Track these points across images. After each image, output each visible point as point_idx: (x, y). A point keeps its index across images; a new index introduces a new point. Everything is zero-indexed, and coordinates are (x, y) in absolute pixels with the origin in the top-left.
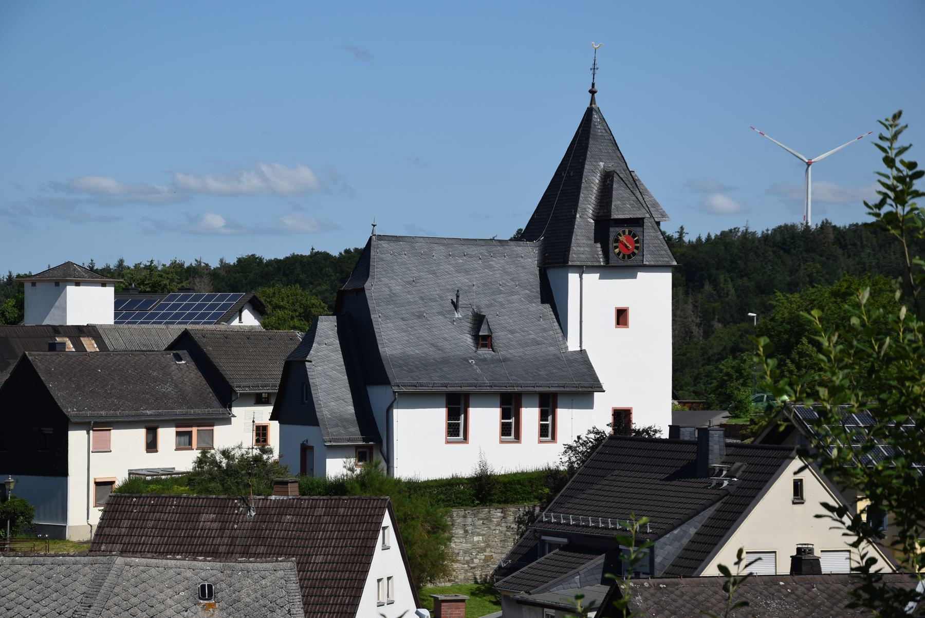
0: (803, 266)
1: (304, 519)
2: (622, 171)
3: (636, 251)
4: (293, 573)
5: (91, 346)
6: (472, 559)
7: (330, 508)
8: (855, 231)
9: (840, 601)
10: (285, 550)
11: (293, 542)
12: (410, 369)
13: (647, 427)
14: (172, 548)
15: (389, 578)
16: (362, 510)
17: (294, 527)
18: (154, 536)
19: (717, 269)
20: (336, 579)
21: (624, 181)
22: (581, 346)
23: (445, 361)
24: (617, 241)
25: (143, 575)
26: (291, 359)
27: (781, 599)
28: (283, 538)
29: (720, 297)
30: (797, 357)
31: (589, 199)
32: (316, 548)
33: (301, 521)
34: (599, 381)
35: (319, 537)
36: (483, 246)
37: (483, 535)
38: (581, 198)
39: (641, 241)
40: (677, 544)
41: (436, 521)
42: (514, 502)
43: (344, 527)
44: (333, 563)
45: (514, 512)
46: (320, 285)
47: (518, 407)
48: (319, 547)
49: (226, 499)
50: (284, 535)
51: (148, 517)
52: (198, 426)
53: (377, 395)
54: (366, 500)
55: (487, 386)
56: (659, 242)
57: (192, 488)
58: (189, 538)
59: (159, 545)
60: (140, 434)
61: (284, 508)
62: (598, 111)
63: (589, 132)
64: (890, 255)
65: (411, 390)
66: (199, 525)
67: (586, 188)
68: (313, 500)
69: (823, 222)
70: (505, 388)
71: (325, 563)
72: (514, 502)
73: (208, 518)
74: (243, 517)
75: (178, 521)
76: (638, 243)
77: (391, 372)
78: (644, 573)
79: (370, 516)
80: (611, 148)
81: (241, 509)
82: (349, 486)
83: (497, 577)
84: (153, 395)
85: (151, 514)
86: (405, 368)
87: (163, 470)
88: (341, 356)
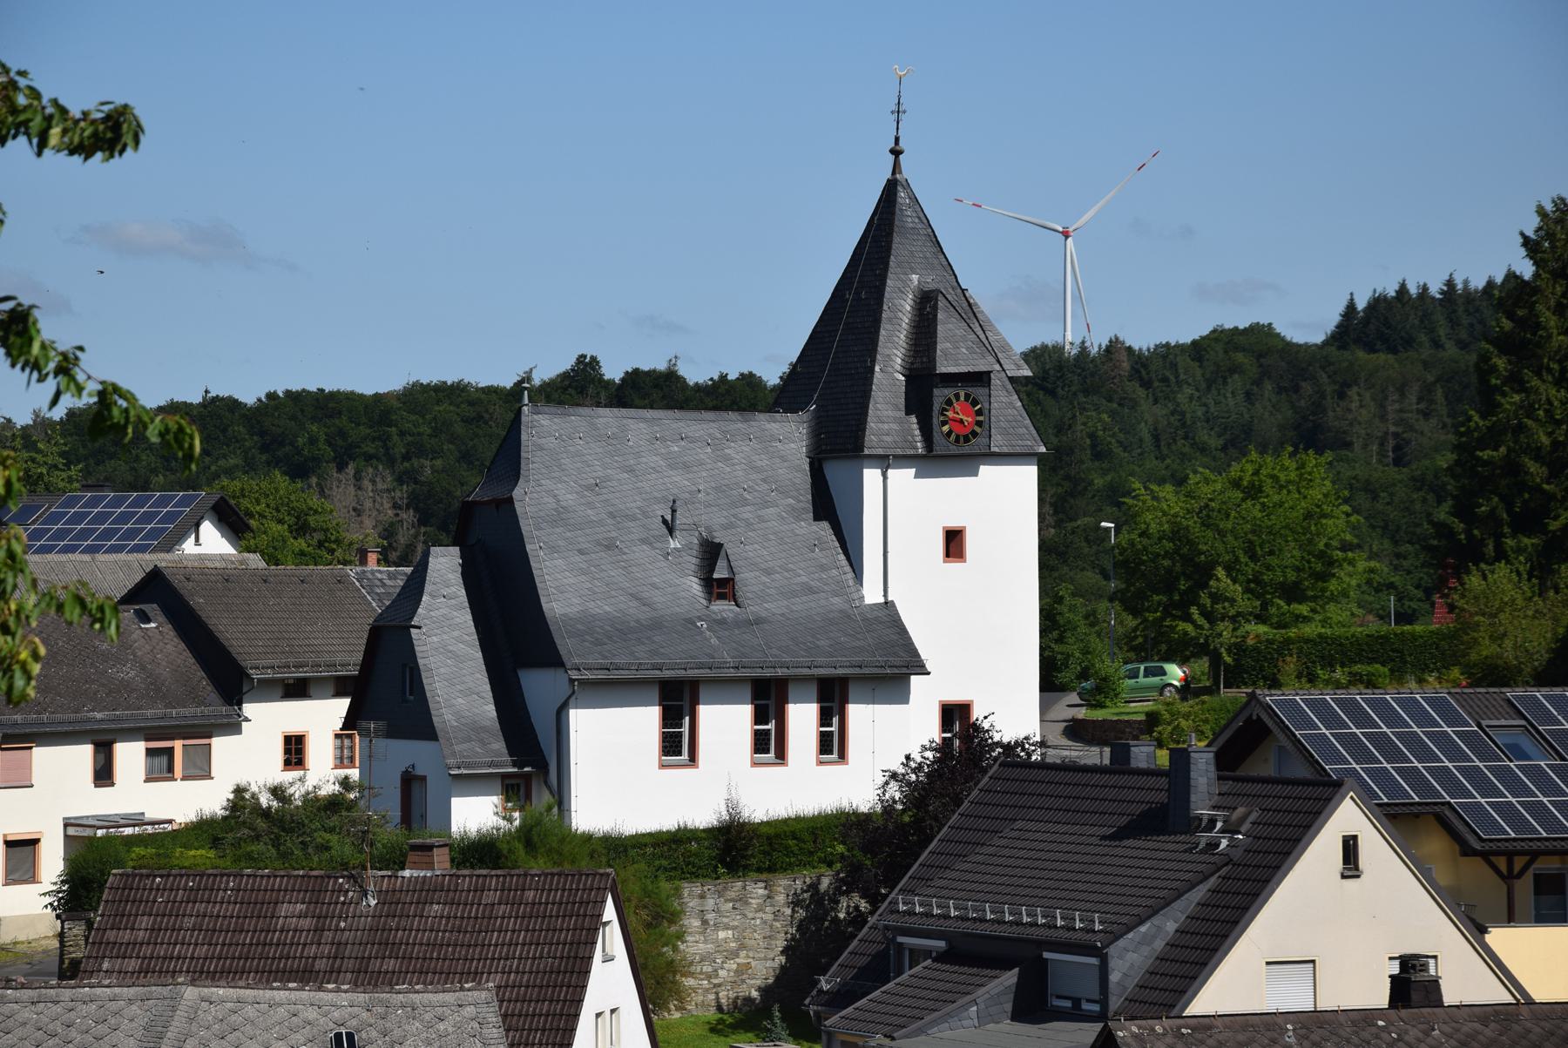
0: (1080, 419)
1: (463, 911)
2: (950, 290)
3: (978, 429)
4: (492, 1009)
6: (716, 971)
7: (510, 890)
8: (1165, 357)
10: (433, 965)
11: (447, 951)
13: (1022, 736)
14: (231, 965)
15: (613, 1011)
16: (566, 894)
17: (447, 925)
18: (196, 944)
20: (527, 1015)
21: (954, 308)
22: (885, 595)
23: (656, 625)
25: (233, 1017)
26: (381, 623)
28: (555, 958)
30: (1208, 602)
31: (896, 339)
32: (488, 961)
33: (459, 915)
34: (919, 656)
35: (493, 942)
37: (734, 928)
38: (881, 338)
39: (987, 412)
40: (1146, 950)
41: (660, 906)
42: (785, 868)
43: (535, 923)
44: (520, 987)
45: (785, 886)
46: (225, 456)
47: (782, 702)
48: (493, 959)
50: (429, 939)
51: (185, 910)
52: (184, 738)
53: (538, 686)
54: (573, 875)
56: (1016, 413)
58: (260, 947)
59: (206, 959)
60: (83, 754)
61: (428, 890)
62: (907, 186)
63: (891, 224)
64: (1226, 397)
65: (601, 675)
66: (277, 924)
67: (890, 320)
68: (478, 876)
69: (1111, 341)
71: (506, 987)
72: (785, 870)
73: (291, 911)
74: (355, 909)
75: (238, 917)
77: (566, 645)
78: (1088, 1001)
79: (581, 903)
80: (929, 250)
81: (351, 894)
82: (504, 847)
83: (815, 1008)
84: (103, 685)
85: (190, 905)
87: (125, 817)
88: (470, 617)
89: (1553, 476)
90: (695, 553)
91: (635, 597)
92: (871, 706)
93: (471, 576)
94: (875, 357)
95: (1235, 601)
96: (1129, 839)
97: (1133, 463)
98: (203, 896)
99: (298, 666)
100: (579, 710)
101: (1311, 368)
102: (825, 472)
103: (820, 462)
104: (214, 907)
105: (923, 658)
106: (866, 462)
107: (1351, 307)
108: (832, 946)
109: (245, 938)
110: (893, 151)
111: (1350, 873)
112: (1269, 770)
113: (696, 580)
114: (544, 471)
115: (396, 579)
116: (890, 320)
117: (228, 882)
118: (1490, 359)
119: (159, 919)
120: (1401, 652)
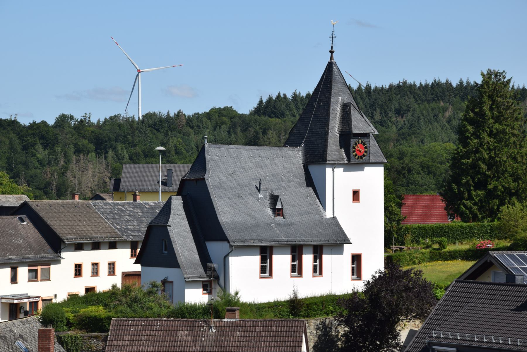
0: (171, 140)
3: (365, 154)
7: (266, 326)
8: (198, 118)
12: (238, 231)
18: (148, 346)
19: (116, 142)
22: (333, 215)
23: (257, 226)
24: (354, 148)
26: (152, 224)
29: (119, 159)
34: (347, 237)
38: (330, 120)
42: (314, 316)
49: (193, 321)
52: (41, 266)
55: (284, 241)
57: (109, 311)
58: (173, 347)
61: (235, 326)
62: (336, 64)
65: (241, 244)
66: (178, 339)
69: (178, 112)
70: (295, 242)
77: (229, 233)
81: (205, 328)
84: (12, 246)
85: (144, 331)
86: (235, 230)
88: (187, 222)
89: (489, 169)
90: (268, 199)
91: (249, 215)
92: (331, 255)
93: (186, 207)
95: (398, 215)
96: (524, 311)
97: (190, 156)
98: (148, 328)
99: (81, 238)
101: (250, 123)
103: (307, 165)
104: (153, 332)
105: (349, 238)
106: (327, 166)
107: (261, 101)
108: (330, 344)
109: (167, 344)
112: (491, 280)
113: (269, 209)
114: (214, 168)
115: (106, 206)
116: (333, 113)
117: (157, 323)
118: (466, 127)
119: (132, 336)
120: (448, 233)
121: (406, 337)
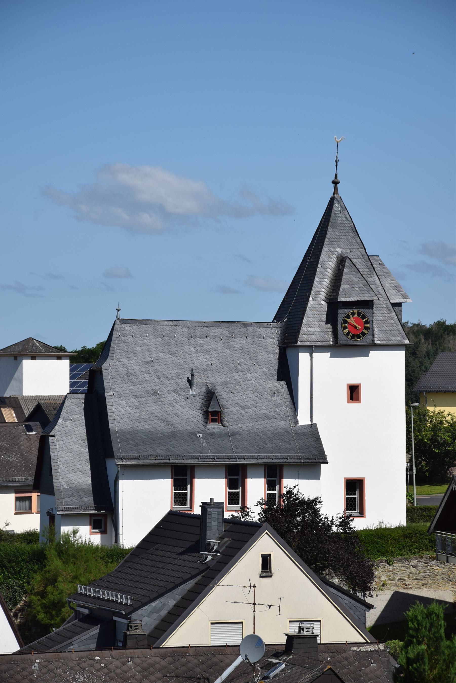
3: (365, 331)
5: (10, 416)
9: (152, 674)
22: (311, 421)
23: (174, 435)
24: (345, 322)
27: (91, 673)
34: (324, 453)
36: (226, 327)
40: (155, 616)
63: (329, 219)
65: (134, 462)
76: (368, 324)
88: (85, 431)
91: (164, 421)
94: (311, 292)
100: (124, 481)
102: (287, 355)
106: (300, 349)
110: (333, 182)
111: (264, 574)
121: (386, 602)
